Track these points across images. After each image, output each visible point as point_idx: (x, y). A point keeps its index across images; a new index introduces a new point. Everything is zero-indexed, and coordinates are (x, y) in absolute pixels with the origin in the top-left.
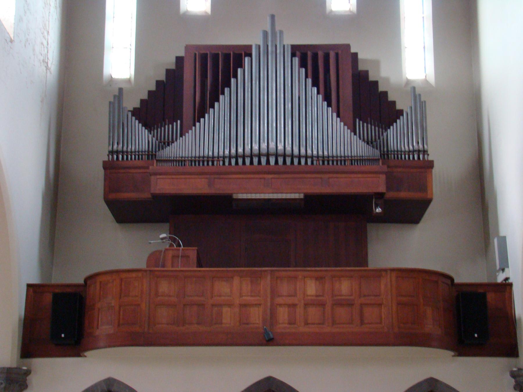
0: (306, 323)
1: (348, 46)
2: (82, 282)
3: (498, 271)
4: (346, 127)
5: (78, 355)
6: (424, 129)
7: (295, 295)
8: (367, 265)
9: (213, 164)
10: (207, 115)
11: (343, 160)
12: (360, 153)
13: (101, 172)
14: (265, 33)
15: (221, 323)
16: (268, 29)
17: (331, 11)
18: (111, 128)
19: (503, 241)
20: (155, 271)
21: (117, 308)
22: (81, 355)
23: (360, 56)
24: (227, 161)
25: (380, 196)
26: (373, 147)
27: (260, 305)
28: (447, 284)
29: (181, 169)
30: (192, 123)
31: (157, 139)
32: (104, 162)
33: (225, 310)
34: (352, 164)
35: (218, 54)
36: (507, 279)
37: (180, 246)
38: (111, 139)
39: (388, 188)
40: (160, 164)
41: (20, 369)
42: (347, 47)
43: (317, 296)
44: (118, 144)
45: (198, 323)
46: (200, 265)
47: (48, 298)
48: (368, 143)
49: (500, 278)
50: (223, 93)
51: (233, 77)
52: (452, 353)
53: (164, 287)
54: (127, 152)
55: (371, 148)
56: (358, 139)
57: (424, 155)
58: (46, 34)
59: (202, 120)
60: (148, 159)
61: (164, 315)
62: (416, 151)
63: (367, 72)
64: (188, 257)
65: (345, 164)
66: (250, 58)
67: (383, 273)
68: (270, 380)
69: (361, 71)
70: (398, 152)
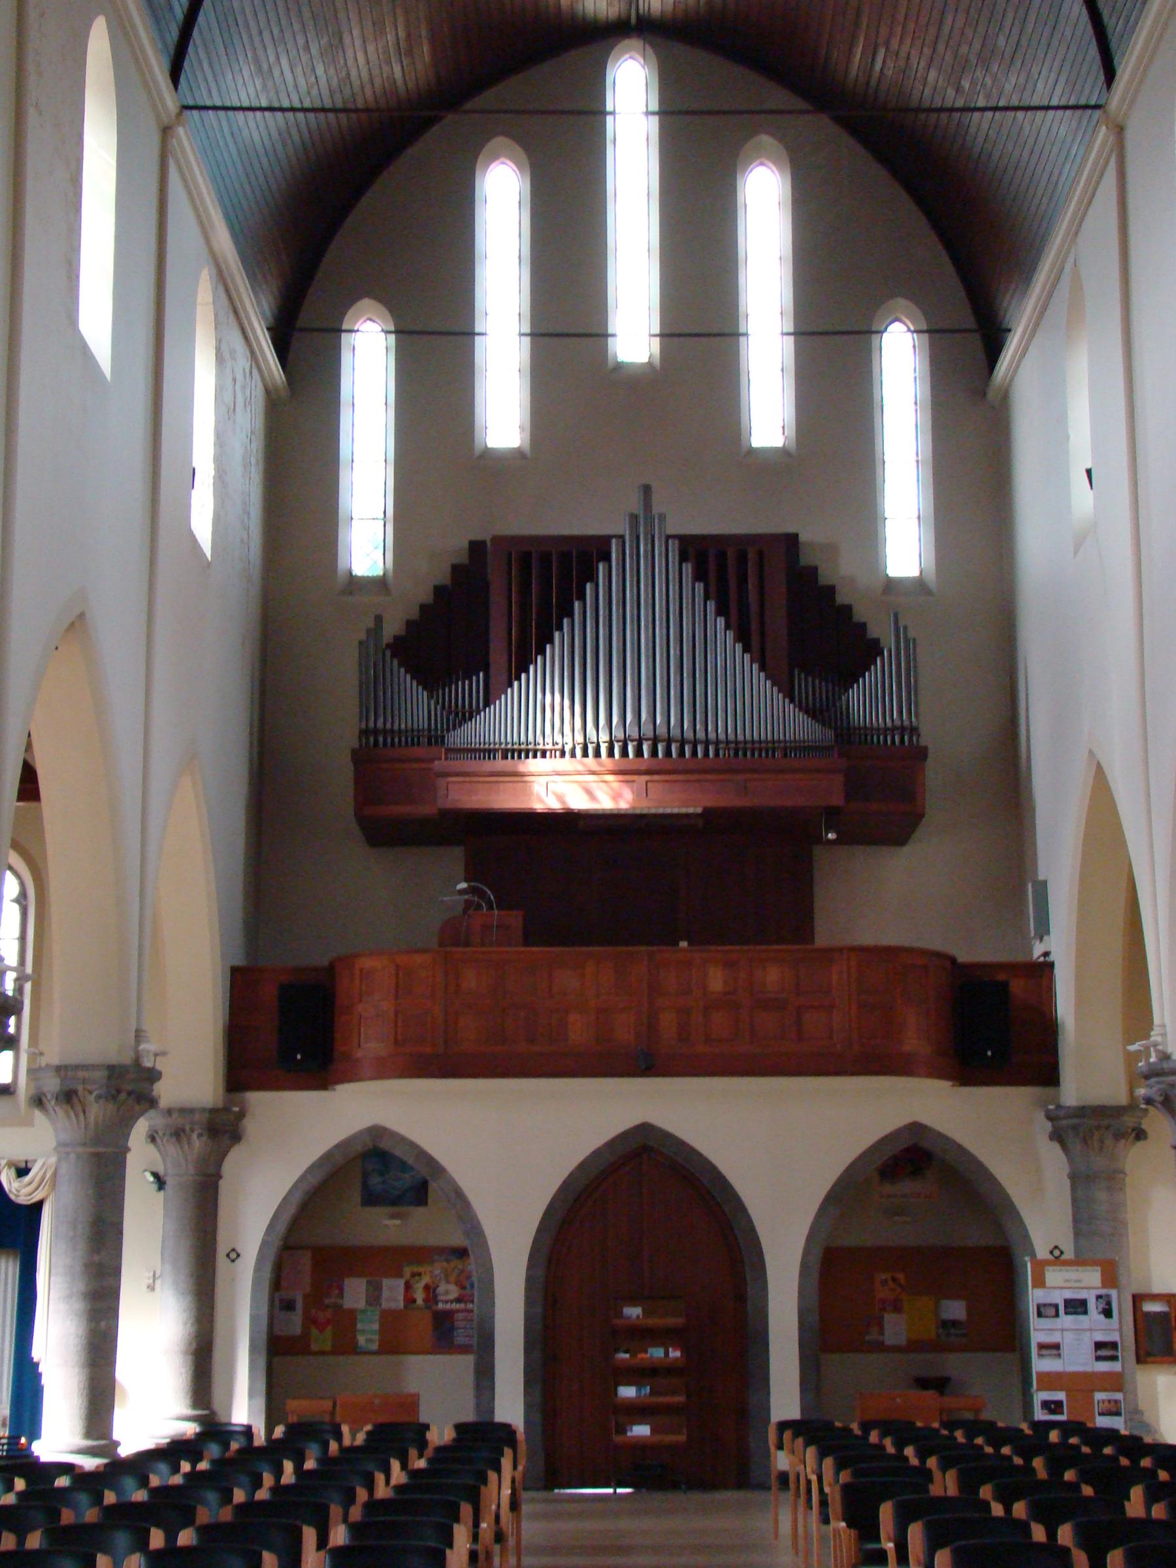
4: (775, 689)
10: (532, 668)
12: (800, 736)
14: (634, 518)
16: (639, 510)
31: (443, 707)
34: (785, 755)
36: (1046, 954)
38: (364, 715)
39: (848, 796)
46: (527, 942)
49: (1038, 950)
51: (578, 599)
54: (392, 731)
55: (818, 727)
60: (430, 743)
65: (774, 756)
68: (645, 1129)
69: (803, 567)
70: (867, 731)
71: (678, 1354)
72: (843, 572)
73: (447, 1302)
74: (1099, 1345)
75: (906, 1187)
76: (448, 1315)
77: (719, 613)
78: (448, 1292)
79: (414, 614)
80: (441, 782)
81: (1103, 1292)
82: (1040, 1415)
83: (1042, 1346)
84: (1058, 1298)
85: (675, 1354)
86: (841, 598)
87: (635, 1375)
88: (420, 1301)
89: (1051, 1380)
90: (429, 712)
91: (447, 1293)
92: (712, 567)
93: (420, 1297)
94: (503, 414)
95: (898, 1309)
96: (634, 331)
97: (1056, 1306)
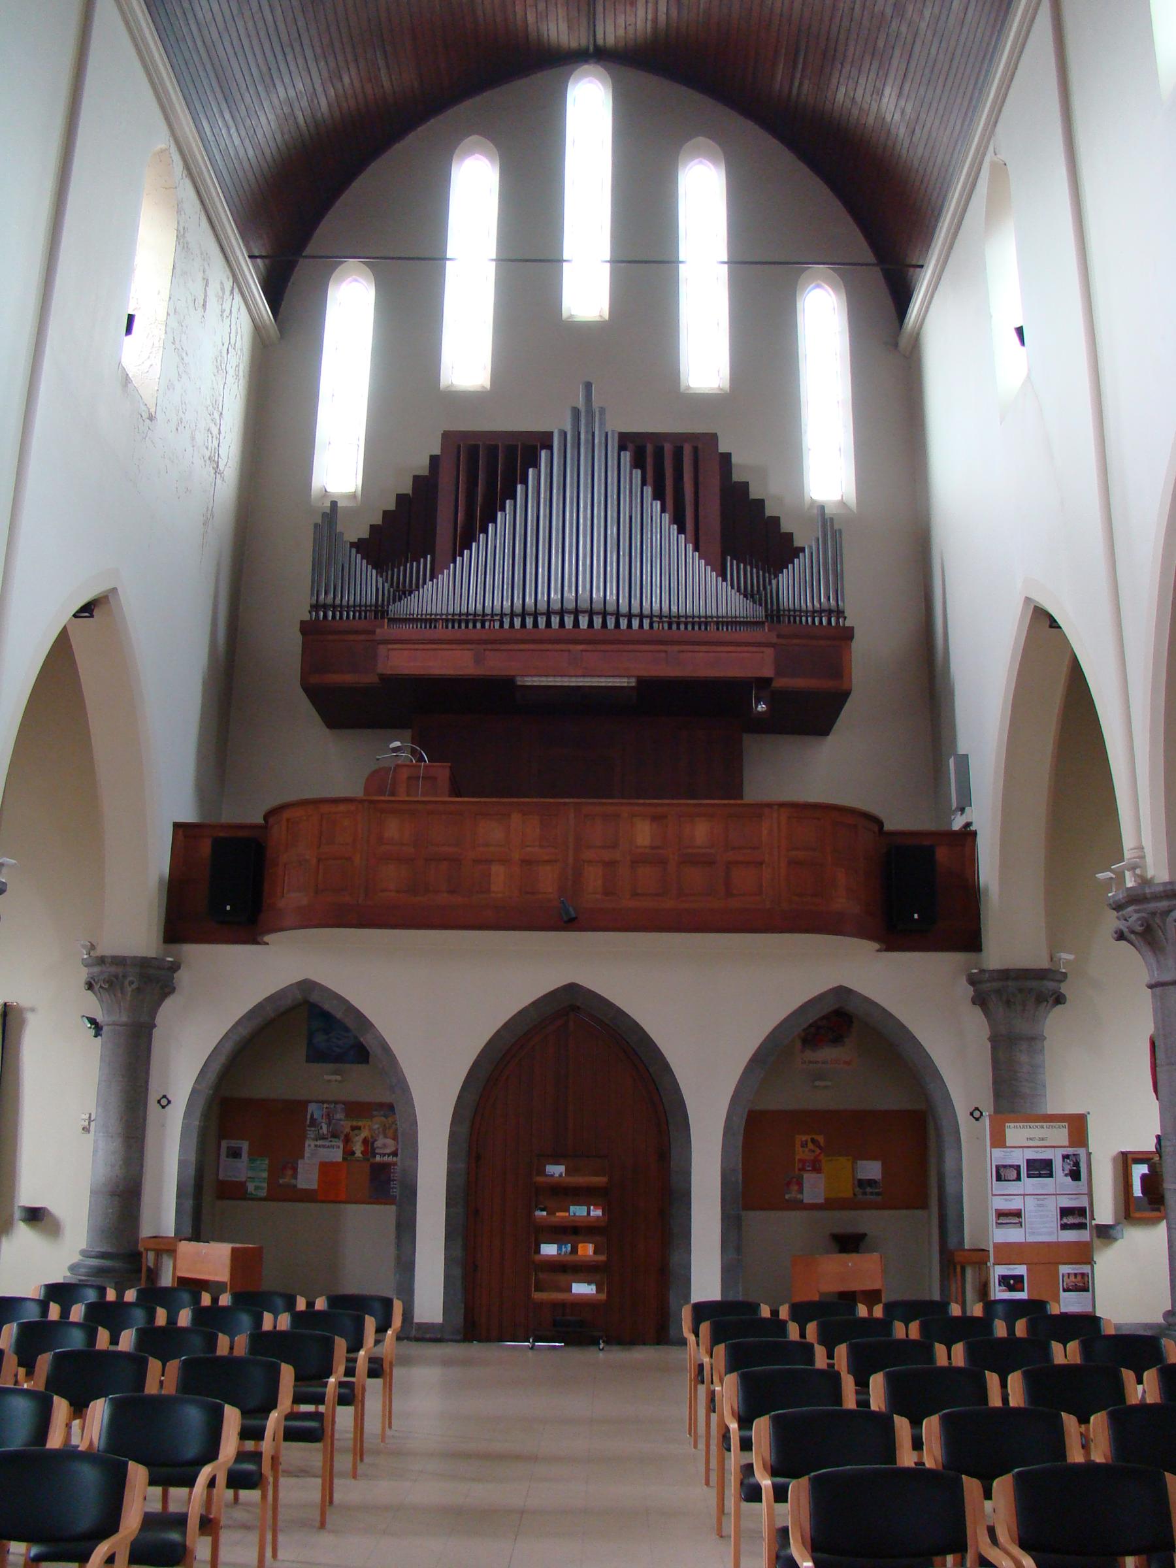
1: (713, 438)
3: (956, 810)
5: (254, 941)
6: (838, 576)
7: (614, 846)
9: (483, 626)
11: (703, 622)
12: (732, 612)
13: (298, 638)
14: (576, 412)
16: (581, 404)
17: (689, 387)
18: (316, 565)
20: (379, 801)
21: (314, 861)
22: (259, 939)
24: (507, 621)
26: (754, 602)
29: (429, 633)
30: (450, 558)
31: (392, 585)
33: (498, 870)
36: (968, 824)
37: (421, 759)
39: (780, 672)
41: (164, 960)
42: (712, 439)
43: (652, 848)
45: (452, 892)
47: (205, 848)
48: (745, 596)
49: (957, 824)
50: (503, 509)
52: (877, 946)
53: (393, 829)
55: (749, 603)
58: (216, 416)
61: (391, 876)
62: (825, 611)
64: (435, 779)
68: (572, 989)
71: (599, 1213)
73: (384, 1155)
74: (1065, 1212)
75: (827, 1053)
76: (385, 1168)
77: (655, 498)
78: (385, 1144)
79: (378, 520)
80: (382, 649)
81: (1070, 1151)
82: (999, 1293)
83: (1001, 1214)
84: (1019, 1158)
85: (597, 1213)
87: (559, 1233)
88: (358, 1154)
89: (1008, 1253)
90: (377, 590)
91: (385, 1146)
92: (649, 461)
93: (358, 1149)
94: (468, 355)
95: (817, 1169)
96: (586, 290)
97: (1018, 1168)
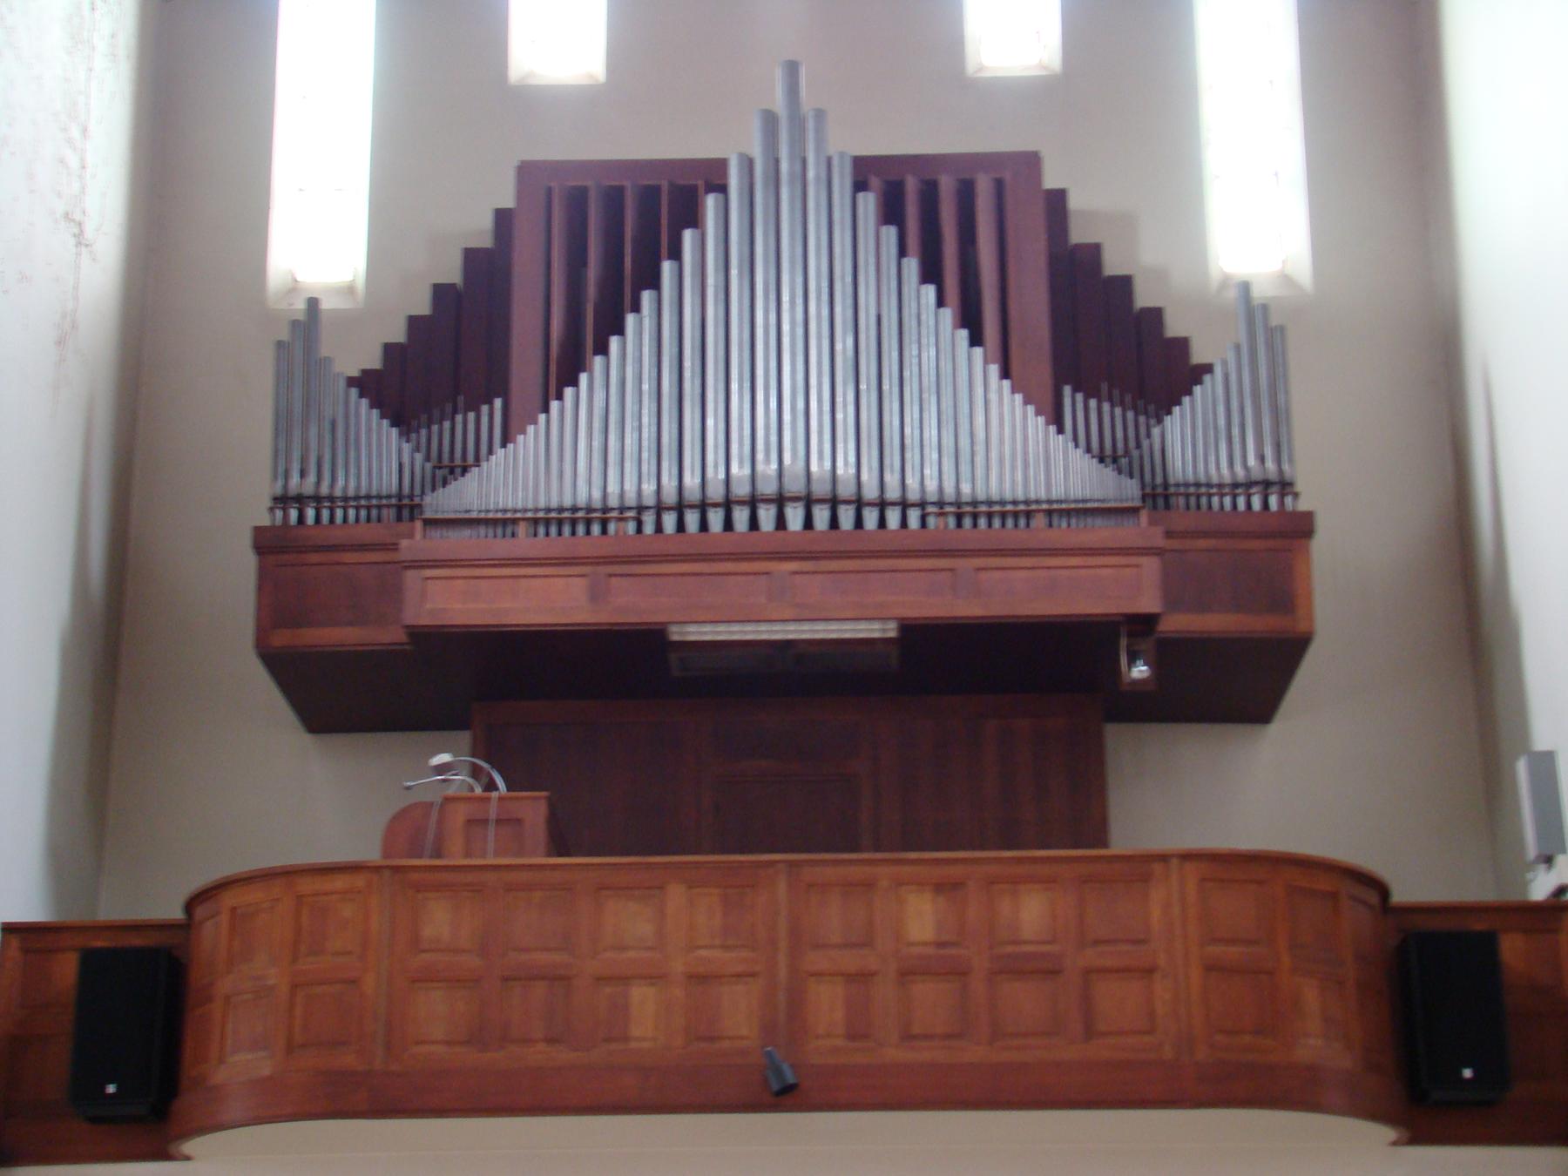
0: (908, 1037)
2: (176, 913)
3: (1530, 866)
4: (1031, 409)
6: (1280, 417)
7: (867, 943)
8: (1103, 842)
11: (1023, 512)
14: (770, 120)
15: (626, 1038)
16: (779, 104)
18: (283, 425)
19: (1545, 765)
23: (1074, 202)
25: (1142, 624)
27: (753, 975)
28: (1364, 903)
31: (428, 458)
32: (259, 532)
33: (643, 998)
35: (620, 190)
37: (491, 786)
38: (280, 454)
39: (1173, 601)
40: (436, 533)
43: (941, 945)
44: (303, 474)
45: (550, 1040)
47: (66, 969)
48: (1102, 460)
50: (636, 308)
51: (670, 257)
52: (1388, 1133)
53: (440, 921)
55: (1109, 472)
56: (1071, 445)
57: (1282, 496)
58: (75, 133)
59: (569, 392)
60: (399, 519)
63: (1095, 250)
64: (519, 821)
66: (721, 196)
67: (1157, 868)
69: (1078, 246)
70: (1198, 491)
72: (1144, 259)
86: (1144, 298)
